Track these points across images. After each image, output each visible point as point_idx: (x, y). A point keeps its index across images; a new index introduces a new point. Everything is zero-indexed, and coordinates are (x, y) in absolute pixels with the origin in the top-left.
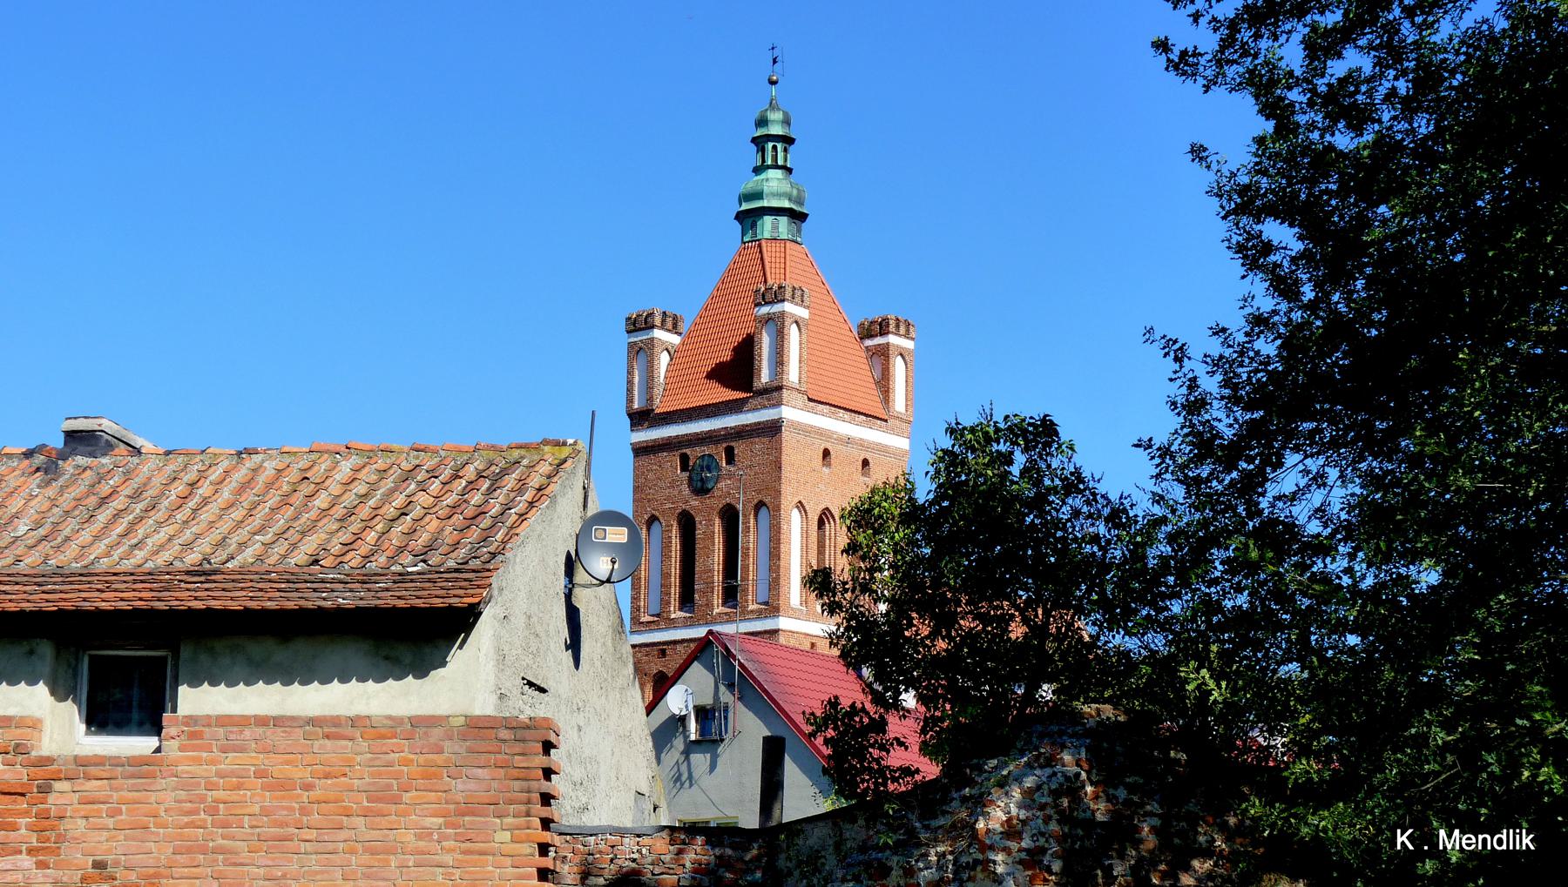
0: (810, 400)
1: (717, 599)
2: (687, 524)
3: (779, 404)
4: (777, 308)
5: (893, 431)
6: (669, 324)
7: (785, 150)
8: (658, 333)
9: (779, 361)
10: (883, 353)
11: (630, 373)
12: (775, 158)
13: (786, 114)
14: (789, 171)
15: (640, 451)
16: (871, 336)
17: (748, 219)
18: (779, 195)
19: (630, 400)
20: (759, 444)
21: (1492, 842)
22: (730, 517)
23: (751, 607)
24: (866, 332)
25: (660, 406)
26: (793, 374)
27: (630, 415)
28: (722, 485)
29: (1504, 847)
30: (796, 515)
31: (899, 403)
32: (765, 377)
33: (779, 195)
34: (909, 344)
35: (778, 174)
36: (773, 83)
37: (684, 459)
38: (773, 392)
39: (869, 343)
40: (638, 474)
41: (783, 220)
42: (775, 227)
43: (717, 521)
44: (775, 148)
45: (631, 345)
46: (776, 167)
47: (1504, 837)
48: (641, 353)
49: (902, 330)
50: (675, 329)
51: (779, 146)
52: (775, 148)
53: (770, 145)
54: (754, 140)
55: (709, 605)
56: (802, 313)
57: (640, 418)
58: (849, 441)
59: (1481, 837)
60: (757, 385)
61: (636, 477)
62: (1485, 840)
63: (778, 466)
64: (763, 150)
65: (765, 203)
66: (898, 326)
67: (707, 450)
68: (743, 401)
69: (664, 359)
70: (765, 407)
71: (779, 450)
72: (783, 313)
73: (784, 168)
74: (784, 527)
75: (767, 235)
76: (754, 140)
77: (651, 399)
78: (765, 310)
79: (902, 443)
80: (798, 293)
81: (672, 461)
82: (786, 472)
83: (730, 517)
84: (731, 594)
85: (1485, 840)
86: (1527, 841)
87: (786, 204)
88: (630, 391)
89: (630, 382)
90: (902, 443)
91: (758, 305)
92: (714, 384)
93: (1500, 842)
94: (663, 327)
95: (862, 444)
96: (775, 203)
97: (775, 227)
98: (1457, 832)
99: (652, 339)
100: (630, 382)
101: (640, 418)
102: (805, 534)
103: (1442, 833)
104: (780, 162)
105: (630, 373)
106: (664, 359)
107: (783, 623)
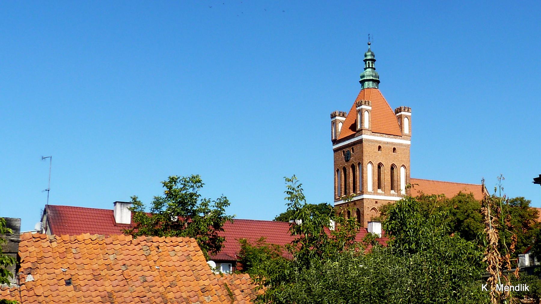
1: (351, 191)
2: (345, 169)
3: (362, 135)
4: (399, 114)
5: (404, 139)
9: (362, 122)
10: (400, 118)
11: (332, 129)
12: (369, 65)
14: (374, 69)
15: (335, 151)
16: (398, 113)
17: (362, 82)
18: (369, 76)
19: (332, 137)
20: (358, 146)
22: (353, 167)
24: (397, 112)
25: (338, 138)
29: (519, 290)
32: (359, 127)
33: (369, 76)
34: (409, 114)
35: (370, 70)
36: (369, 44)
38: (360, 132)
43: (351, 169)
45: (332, 121)
46: (369, 68)
47: (519, 287)
48: (334, 123)
49: (406, 110)
50: (343, 116)
54: (364, 61)
55: (350, 193)
56: (369, 108)
57: (335, 142)
62: (512, 288)
63: (362, 152)
64: (366, 63)
65: (365, 78)
66: (405, 109)
67: (348, 149)
68: (354, 134)
69: (340, 125)
73: (372, 68)
74: (365, 169)
76: (364, 61)
78: (358, 108)
79: (409, 142)
80: (367, 103)
83: (353, 167)
84: (354, 190)
85: (512, 288)
86: (526, 288)
87: (371, 78)
89: (332, 132)
90: (409, 142)
92: (350, 130)
93: (517, 288)
94: (339, 116)
95: (392, 144)
101: (335, 142)
102: (373, 171)
106: (340, 125)
107: (365, 196)
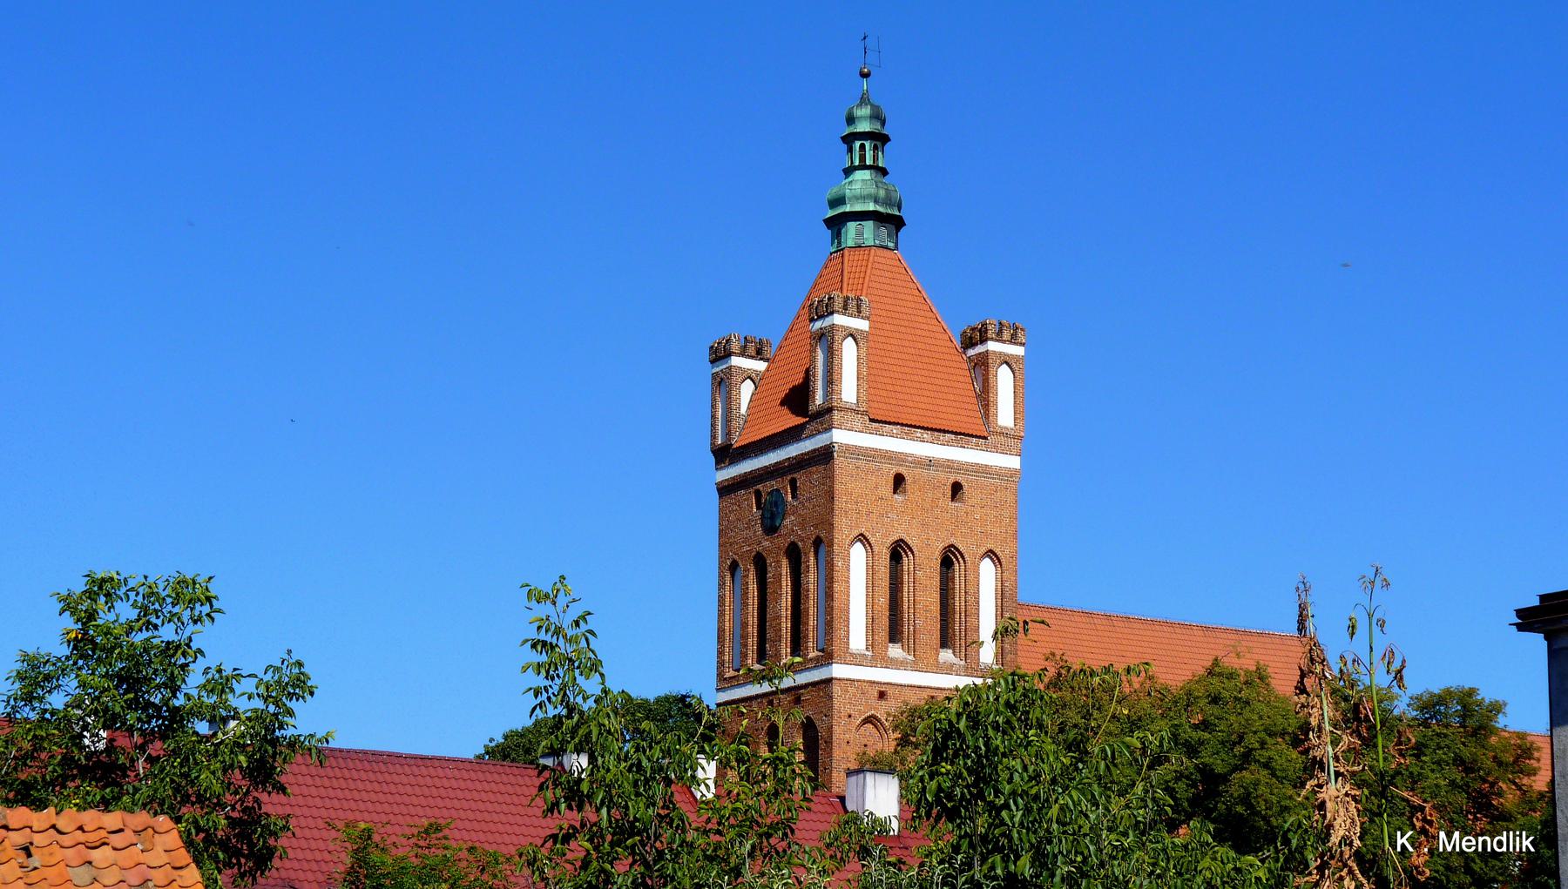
0: (872, 420)
1: (785, 649)
3: (829, 429)
4: (827, 322)
6: (751, 350)
7: (875, 148)
8: (736, 361)
9: (831, 380)
10: (982, 366)
11: (713, 406)
12: (862, 158)
13: (875, 108)
14: (884, 172)
15: (725, 490)
17: (836, 224)
18: (863, 198)
19: (714, 437)
20: (816, 473)
21: (1492, 844)
22: (794, 555)
23: (811, 655)
24: (968, 342)
25: (738, 441)
26: (848, 390)
27: (714, 452)
28: (787, 522)
29: (1504, 849)
30: (858, 553)
31: (1005, 415)
32: (819, 398)
33: (863, 198)
36: (865, 75)
37: (758, 494)
39: (971, 352)
40: (723, 515)
41: (869, 225)
42: (860, 234)
44: (862, 147)
45: (714, 376)
46: (863, 167)
47: (1504, 839)
48: (723, 384)
49: (1006, 335)
50: (759, 354)
51: (867, 144)
52: (862, 147)
53: (857, 144)
55: (778, 656)
56: (862, 325)
58: (930, 463)
59: (1481, 839)
60: (812, 408)
61: (721, 519)
62: (1484, 842)
63: (830, 496)
64: (850, 150)
65: (848, 208)
67: (773, 484)
68: (801, 427)
69: (747, 389)
70: (819, 433)
71: (832, 478)
72: (833, 326)
75: (850, 243)
77: (728, 434)
78: (818, 325)
81: (747, 498)
82: (841, 502)
84: (797, 647)
85: (1484, 842)
87: (871, 207)
88: (713, 426)
89: (714, 417)
90: (1014, 462)
91: (812, 320)
92: (785, 410)
93: (1500, 844)
94: (743, 354)
95: (949, 465)
96: (858, 207)
97: (860, 234)
98: (1457, 834)
99: (730, 368)
100: (714, 417)
102: (871, 570)
103: (1442, 835)
104: (869, 162)
105: (713, 406)
106: (747, 389)
107: (838, 670)
